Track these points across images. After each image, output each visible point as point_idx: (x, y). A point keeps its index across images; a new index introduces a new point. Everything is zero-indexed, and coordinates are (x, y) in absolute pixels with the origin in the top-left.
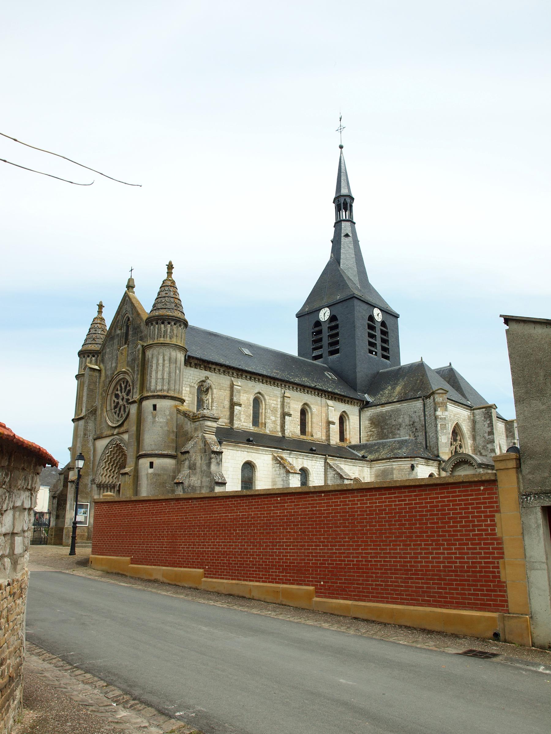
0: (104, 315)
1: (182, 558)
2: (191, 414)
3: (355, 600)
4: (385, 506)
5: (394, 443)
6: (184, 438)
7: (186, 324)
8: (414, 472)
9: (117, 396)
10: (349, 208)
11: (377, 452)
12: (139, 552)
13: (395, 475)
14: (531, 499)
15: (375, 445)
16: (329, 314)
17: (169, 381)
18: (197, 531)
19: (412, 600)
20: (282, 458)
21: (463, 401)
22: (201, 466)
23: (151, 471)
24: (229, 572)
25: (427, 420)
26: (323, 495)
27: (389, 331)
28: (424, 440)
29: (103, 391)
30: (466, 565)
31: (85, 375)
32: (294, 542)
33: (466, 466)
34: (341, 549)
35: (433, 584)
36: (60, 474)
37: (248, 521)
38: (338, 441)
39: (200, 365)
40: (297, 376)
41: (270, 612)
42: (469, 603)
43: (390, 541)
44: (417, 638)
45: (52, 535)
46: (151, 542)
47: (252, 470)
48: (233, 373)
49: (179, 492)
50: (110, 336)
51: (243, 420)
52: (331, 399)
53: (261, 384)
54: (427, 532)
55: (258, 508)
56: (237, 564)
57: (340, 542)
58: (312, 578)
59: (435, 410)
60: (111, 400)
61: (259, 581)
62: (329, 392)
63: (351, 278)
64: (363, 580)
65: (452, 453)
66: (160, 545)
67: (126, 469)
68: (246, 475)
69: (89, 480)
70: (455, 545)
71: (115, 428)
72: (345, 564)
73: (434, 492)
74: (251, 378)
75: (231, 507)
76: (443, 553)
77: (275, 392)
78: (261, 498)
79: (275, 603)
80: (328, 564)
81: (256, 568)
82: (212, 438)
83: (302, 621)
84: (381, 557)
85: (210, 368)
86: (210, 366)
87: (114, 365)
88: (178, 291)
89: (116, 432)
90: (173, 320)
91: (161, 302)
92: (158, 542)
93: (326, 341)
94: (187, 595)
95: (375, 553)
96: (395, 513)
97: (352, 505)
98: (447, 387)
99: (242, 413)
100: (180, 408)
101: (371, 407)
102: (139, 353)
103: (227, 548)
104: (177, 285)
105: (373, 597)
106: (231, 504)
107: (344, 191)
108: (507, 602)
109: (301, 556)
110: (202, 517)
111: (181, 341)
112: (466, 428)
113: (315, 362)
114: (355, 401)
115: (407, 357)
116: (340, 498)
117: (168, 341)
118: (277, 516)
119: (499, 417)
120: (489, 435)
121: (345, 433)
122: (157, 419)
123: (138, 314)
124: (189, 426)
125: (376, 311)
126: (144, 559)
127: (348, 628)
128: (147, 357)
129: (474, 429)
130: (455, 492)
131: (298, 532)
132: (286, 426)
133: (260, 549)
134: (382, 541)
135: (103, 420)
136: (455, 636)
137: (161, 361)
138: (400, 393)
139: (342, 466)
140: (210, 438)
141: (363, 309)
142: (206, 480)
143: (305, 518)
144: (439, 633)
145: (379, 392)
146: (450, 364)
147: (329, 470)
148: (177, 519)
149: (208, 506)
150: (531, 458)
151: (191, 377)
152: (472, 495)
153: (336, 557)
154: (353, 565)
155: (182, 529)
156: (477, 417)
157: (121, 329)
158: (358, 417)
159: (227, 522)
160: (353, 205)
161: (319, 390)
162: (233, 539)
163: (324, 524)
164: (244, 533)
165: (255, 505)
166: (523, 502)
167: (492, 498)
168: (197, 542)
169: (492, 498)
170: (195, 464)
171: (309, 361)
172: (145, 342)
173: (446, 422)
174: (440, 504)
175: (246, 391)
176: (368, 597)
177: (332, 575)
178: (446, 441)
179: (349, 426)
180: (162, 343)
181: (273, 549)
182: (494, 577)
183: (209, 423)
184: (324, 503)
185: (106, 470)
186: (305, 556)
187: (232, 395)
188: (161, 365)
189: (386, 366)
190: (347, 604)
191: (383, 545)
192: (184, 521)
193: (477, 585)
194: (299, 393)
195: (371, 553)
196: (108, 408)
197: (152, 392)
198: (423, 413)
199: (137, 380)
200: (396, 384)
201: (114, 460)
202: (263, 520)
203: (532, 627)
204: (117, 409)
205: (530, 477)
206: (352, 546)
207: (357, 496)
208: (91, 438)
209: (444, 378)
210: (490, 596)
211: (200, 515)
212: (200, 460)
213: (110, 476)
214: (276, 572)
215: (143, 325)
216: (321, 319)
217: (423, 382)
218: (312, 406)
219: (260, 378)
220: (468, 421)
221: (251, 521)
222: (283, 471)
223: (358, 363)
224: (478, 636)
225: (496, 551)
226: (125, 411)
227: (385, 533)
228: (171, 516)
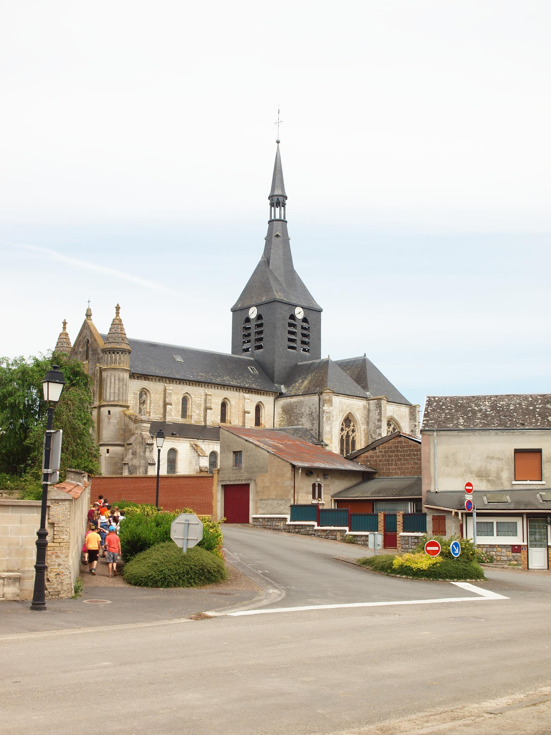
20: (196, 445)
23: (108, 455)
51: (173, 414)
52: (248, 393)
74: (180, 382)
90: (120, 351)
91: (112, 337)
93: (253, 337)
99: (173, 409)
100: (126, 413)
117: (117, 366)
124: (132, 426)
137: (113, 381)
141: (285, 311)
142: (142, 462)
145: (292, 384)
146: (365, 355)
170: (136, 452)
175: (176, 392)
183: (145, 425)
187: (165, 397)
189: (304, 359)
197: (107, 402)
200: (305, 378)
218: (231, 400)
222: (196, 454)
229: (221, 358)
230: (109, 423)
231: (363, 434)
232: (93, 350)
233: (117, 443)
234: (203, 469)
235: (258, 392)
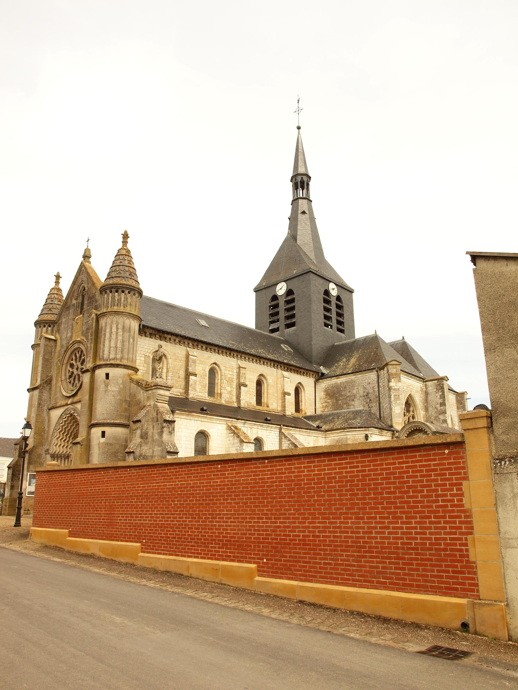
0: (61, 286)
1: (119, 531)
2: (144, 383)
3: (301, 580)
4: (335, 473)
5: (349, 413)
6: (136, 407)
7: (140, 293)
9: (72, 366)
10: (306, 187)
11: (332, 422)
12: (77, 524)
14: (505, 464)
15: (330, 415)
16: (286, 288)
18: (135, 502)
19: (366, 581)
20: (236, 428)
21: (416, 373)
22: (153, 435)
23: (103, 440)
24: (167, 547)
26: (266, 461)
27: (344, 305)
28: (378, 411)
29: (59, 361)
30: (428, 542)
31: (41, 345)
32: (234, 514)
33: (421, 435)
34: (285, 523)
35: (390, 563)
36: (15, 444)
37: (187, 491)
38: (294, 411)
39: (155, 335)
40: (253, 348)
41: (205, 594)
42: (432, 587)
43: (341, 514)
44: (371, 628)
45: (6, 506)
46: (89, 513)
47: (206, 440)
48: (188, 343)
49: (130, 461)
50: (66, 306)
51: (198, 390)
52: (287, 371)
53: (217, 355)
54: (382, 503)
55: (197, 476)
56: (175, 538)
57: (285, 514)
58: (254, 554)
59: (389, 381)
60: (66, 369)
61: (197, 557)
62: (284, 364)
63: (307, 253)
64: (310, 558)
65: (405, 423)
66: (98, 516)
67: (78, 439)
68: (200, 445)
69: (43, 450)
70: (416, 518)
71: (69, 397)
72: (290, 540)
73: (391, 457)
75: (170, 476)
76: (402, 528)
77: (231, 362)
78: (200, 466)
79: (214, 582)
80: (272, 539)
81: (195, 542)
82: (164, 407)
83: (240, 605)
84: (330, 532)
85: (166, 338)
86: (166, 336)
87: (69, 335)
88: (133, 260)
89: (70, 401)
92: (96, 514)
93: (282, 315)
94: (120, 572)
95: (323, 527)
96: (347, 482)
97: (298, 472)
98: (401, 359)
99: (198, 383)
100: (133, 377)
101: (326, 378)
102: (93, 322)
103: (165, 521)
104: (132, 254)
105: (321, 577)
106: (170, 472)
107: (301, 170)
108: (478, 586)
109: (243, 530)
110: (140, 487)
111: (135, 310)
112: (418, 399)
113: (271, 335)
114: (311, 373)
115: (361, 330)
116: (285, 465)
117: (122, 309)
118: (217, 486)
120: (441, 406)
122: (109, 388)
123: (94, 284)
124: (142, 395)
125: (332, 286)
126: (81, 532)
127: (292, 614)
128: (100, 326)
129: (426, 400)
130: (415, 456)
131: (239, 503)
133: (199, 522)
134: (332, 514)
135: (58, 390)
136: (417, 626)
137: (114, 330)
138: (354, 365)
139: (297, 436)
140: (162, 407)
143: (247, 488)
144: (397, 622)
146: (403, 338)
147: (283, 440)
148: (115, 488)
149: (146, 475)
150: (504, 415)
151: (146, 347)
152: (435, 460)
153: (280, 531)
154: (299, 540)
155: (120, 500)
156: (429, 388)
157: (77, 299)
158: (314, 389)
159: (166, 492)
160: (310, 183)
161: (274, 361)
162: (171, 511)
163: (268, 494)
164: (183, 504)
165: (194, 473)
166: (496, 467)
167: (459, 463)
168: (134, 514)
169: (459, 463)
170: (146, 434)
171: (266, 333)
172: (99, 311)
174: (397, 471)
176: (315, 577)
177: (276, 552)
178: (399, 411)
179: (305, 397)
180: (115, 312)
181: (213, 522)
182: (461, 556)
183: (162, 392)
184: (268, 471)
185: (61, 440)
186: (247, 530)
187: (187, 365)
188: (114, 333)
190: (293, 585)
191: (333, 518)
192: (122, 491)
193: (441, 566)
194: (255, 364)
195: (319, 527)
196: (63, 378)
198: (376, 385)
199: (91, 349)
200: (351, 356)
201: (68, 430)
202: (203, 490)
203: (508, 617)
204: (72, 379)
205: (504, 437)
206: (298, 518)
207: (304, 463)
208: (46, 408)
209: (398, 352)
210: (457, 578)
211: (138, 484)
213: (64, 446)
214: (215, 548)
215: (98, 293)
216: (278, 293)
217: (377, 355)
218: (268, 377)
219: (216, 348)
221: (190, 491)
222: (237, 440)
224: (443, 626)
225: (463, 526)
226: (79, 380)
227: (335, 505)
228: (110, 486)
229: (241, 331)
230: (106, 391)
232: (90, 298)
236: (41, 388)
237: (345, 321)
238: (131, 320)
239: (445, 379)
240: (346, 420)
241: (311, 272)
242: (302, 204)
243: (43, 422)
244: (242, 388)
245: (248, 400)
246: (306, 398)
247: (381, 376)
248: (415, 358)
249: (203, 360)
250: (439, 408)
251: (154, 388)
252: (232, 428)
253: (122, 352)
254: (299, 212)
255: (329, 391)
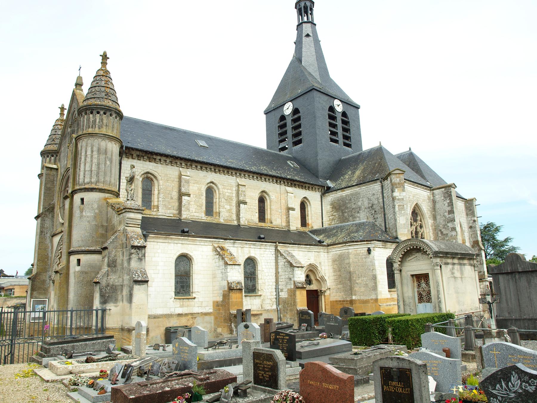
7: (119, 115)
8: (371, 255)
13: (351, 260)
15: (334, 229)
17: (98, 173)
20: (222, 249)
23: (78, 268)
25: (385, 202)
27: (350, 121)
28: (383, 222)
33: (419, 255)
38: (299, 225)
48: (181, 164)
52: (291, 186)
53: (213, 173)
59: (393, 191)
62: (288, 179)
68: (182, 269)
69: (48, 276)
77: (229, 181)
85: (155, 159)
86: (155, 157)
87: (66, 162)
98: (406, 168)
99: (192, 203)
100: (109, 201)
101: (332, 192)
112: (426, 208)
113: (282, 153)
114: (316, 187)
115: (368, 143)
117: (97, 131)
119: (459, 197)
120: (449, 214)
121: (307, 219)
122: (84, 214)
124: (116, 219)
125: (336, 102)
129: (434, 209)
132: (241, 214)
137: (89, 153)
138: (359, 177)
142: (126, 277)
145: (340, 177)
146: (410, 149)
147: (279, 258)
158: (320, 203)
171: (276, 152)
173: (404, 202)
178: (404, 222)
179: (311, 211)
180: (89, 134)
183: (132, 215)
187: (180, 186)
188: (89, 156)
194: (256, 181)
198: (381, 195)
200: (356, 169)
208: (48, 235)
209: (405, 163)
212: (121, 256)
217: (381, 165)
218: (270, 194)
219: (212, 167)
220: (428, 201)
222: (222, 263)
223: (320, 151)
229: (257, 152)
230: (81, 217)
231: (431, 230)
233: (92, 248)
234: (234, 286)
235: (302, 185)
236: (43, 216)
237: (352, 136)
238: (107, 141)
239: (453, 186)
240: (349, 234)
241: (314, 89)
242: (306, 28)
243: (46, 249)
244: (242, 206)
245: (249, 217)
246: (313, 212)
247: (385, 187)
248: (421, 167)
249: (197, 181)
250: (447, 216)
251: (123, 211)
252: (218, 249)
253: (98, 174)
254: (304, 35)
255: (335, 204)
